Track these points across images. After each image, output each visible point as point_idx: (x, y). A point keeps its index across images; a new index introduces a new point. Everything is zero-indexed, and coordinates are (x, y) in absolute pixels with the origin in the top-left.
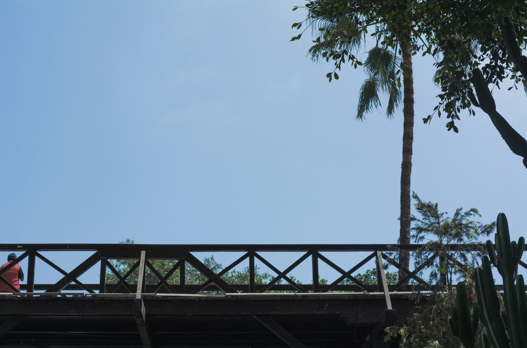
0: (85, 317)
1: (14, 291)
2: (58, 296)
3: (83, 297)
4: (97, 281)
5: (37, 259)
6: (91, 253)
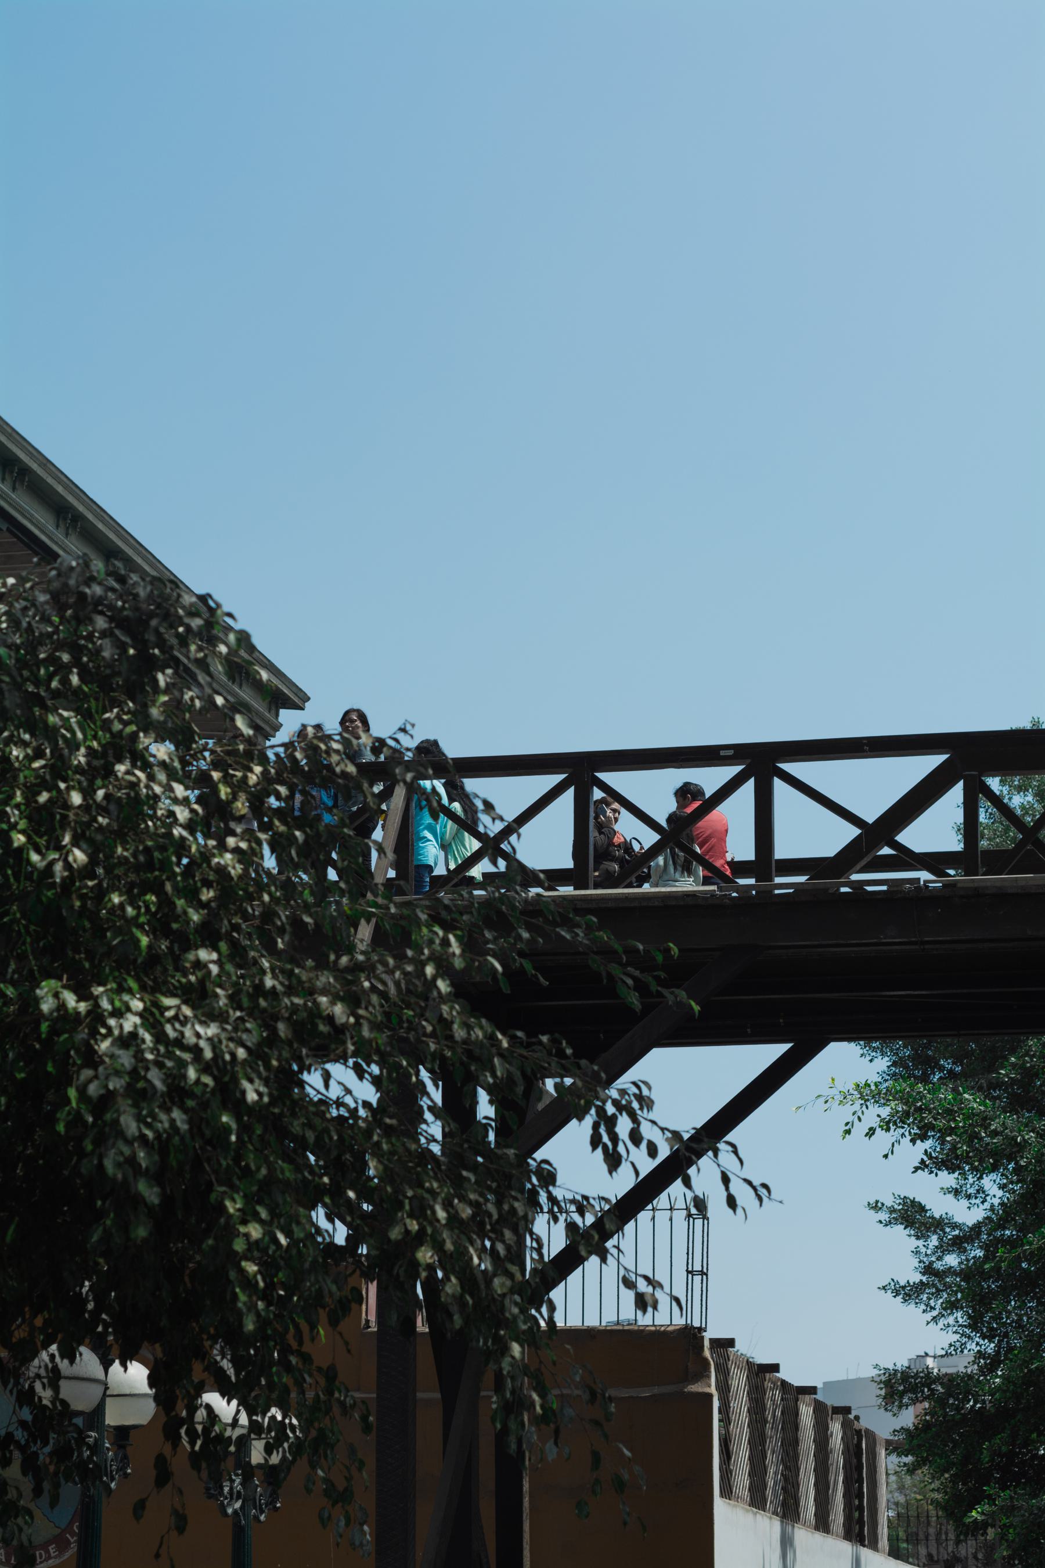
0: (927, 947)
1: (720, 882)
2: (843, 890)
3: (918, 888)
4: (954, 844)
5: (778, 784)
6: (930, 762)
